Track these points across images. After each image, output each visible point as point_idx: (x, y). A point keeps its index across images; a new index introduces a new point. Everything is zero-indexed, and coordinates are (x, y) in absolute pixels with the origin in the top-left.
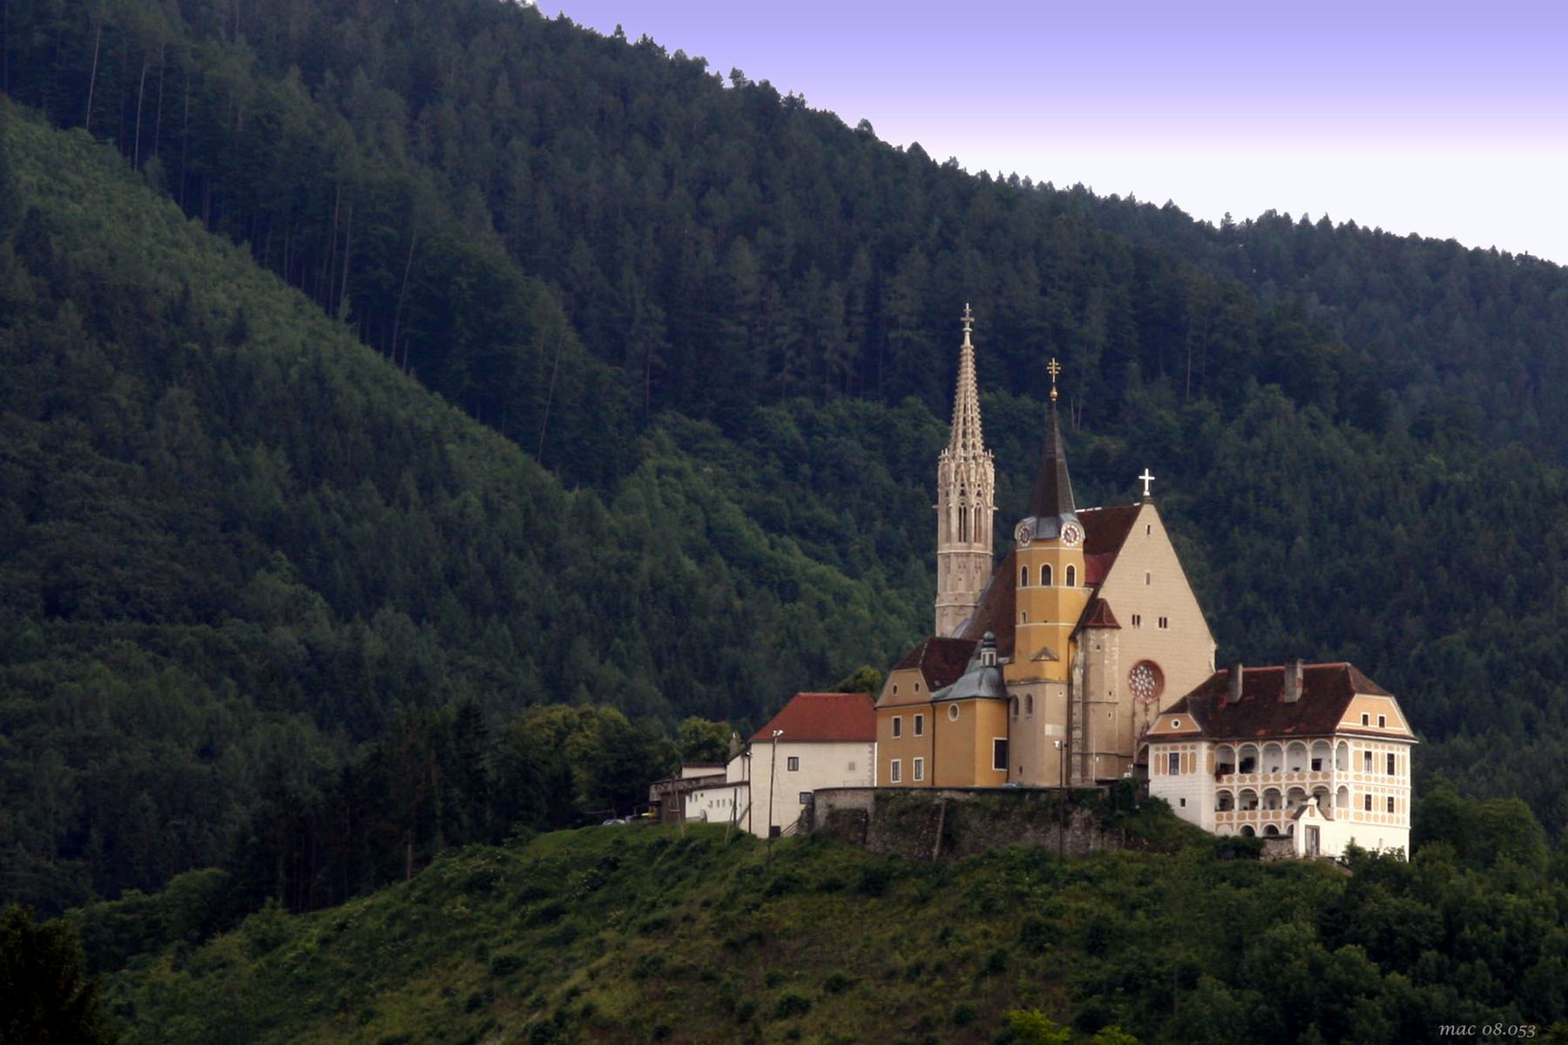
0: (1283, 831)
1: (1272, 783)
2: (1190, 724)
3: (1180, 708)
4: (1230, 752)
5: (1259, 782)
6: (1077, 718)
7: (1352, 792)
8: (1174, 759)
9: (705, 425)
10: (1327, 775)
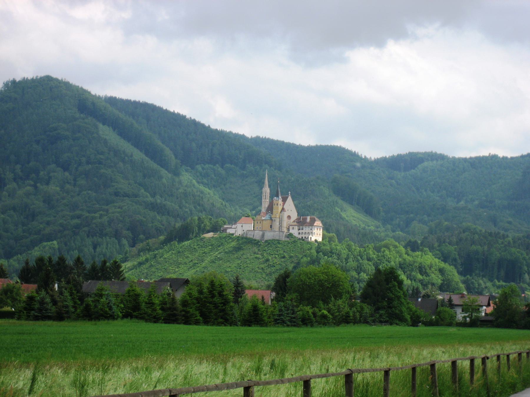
0: (307, 237)
1: (305, 231)
2: (295, 223)
3: (294, 221)
4: (300, 227)
5: (304, 231)
6: (281, 222)
7: (315, 233)
8: (293, 228)
9: (189, 168)
10: (313, 231)
